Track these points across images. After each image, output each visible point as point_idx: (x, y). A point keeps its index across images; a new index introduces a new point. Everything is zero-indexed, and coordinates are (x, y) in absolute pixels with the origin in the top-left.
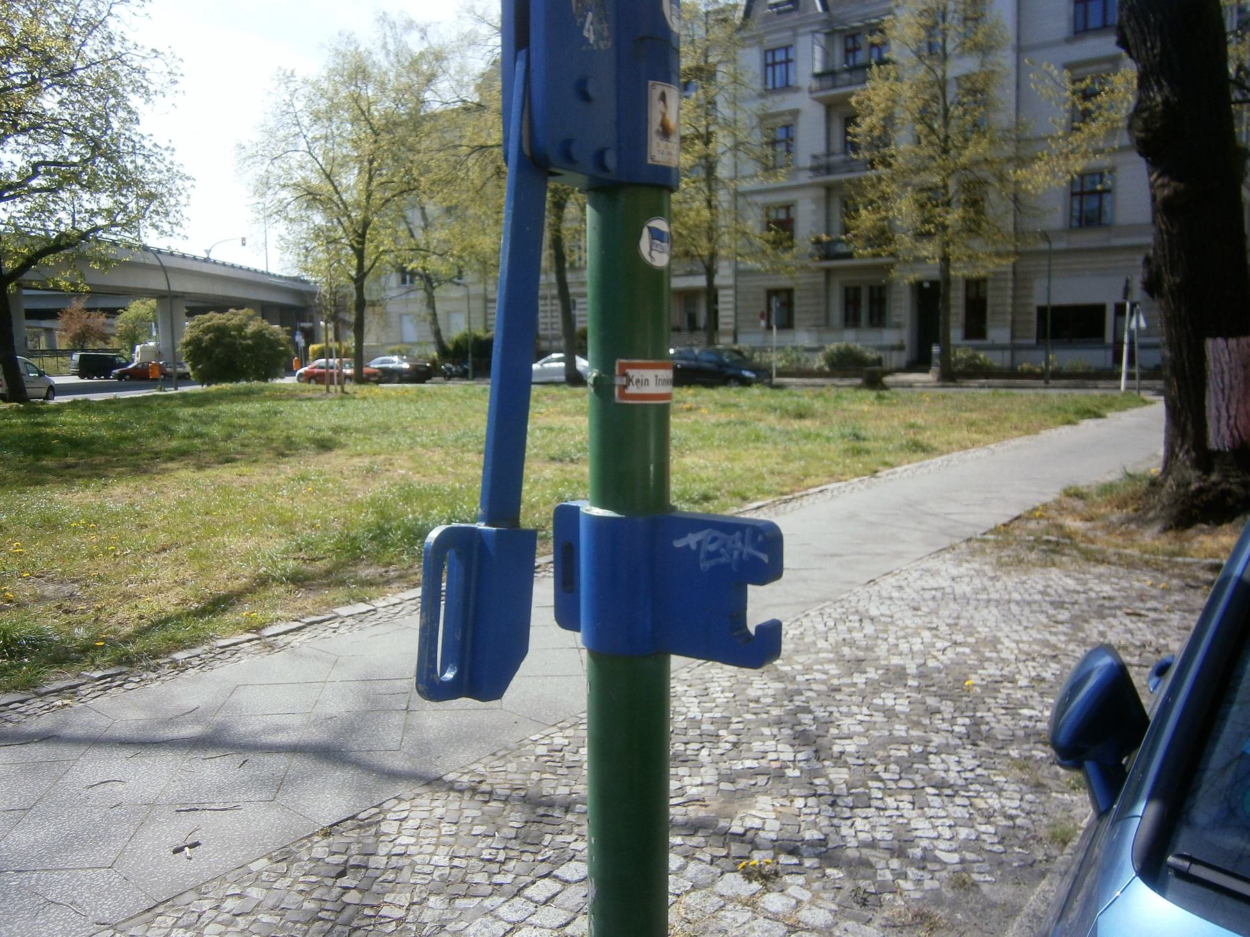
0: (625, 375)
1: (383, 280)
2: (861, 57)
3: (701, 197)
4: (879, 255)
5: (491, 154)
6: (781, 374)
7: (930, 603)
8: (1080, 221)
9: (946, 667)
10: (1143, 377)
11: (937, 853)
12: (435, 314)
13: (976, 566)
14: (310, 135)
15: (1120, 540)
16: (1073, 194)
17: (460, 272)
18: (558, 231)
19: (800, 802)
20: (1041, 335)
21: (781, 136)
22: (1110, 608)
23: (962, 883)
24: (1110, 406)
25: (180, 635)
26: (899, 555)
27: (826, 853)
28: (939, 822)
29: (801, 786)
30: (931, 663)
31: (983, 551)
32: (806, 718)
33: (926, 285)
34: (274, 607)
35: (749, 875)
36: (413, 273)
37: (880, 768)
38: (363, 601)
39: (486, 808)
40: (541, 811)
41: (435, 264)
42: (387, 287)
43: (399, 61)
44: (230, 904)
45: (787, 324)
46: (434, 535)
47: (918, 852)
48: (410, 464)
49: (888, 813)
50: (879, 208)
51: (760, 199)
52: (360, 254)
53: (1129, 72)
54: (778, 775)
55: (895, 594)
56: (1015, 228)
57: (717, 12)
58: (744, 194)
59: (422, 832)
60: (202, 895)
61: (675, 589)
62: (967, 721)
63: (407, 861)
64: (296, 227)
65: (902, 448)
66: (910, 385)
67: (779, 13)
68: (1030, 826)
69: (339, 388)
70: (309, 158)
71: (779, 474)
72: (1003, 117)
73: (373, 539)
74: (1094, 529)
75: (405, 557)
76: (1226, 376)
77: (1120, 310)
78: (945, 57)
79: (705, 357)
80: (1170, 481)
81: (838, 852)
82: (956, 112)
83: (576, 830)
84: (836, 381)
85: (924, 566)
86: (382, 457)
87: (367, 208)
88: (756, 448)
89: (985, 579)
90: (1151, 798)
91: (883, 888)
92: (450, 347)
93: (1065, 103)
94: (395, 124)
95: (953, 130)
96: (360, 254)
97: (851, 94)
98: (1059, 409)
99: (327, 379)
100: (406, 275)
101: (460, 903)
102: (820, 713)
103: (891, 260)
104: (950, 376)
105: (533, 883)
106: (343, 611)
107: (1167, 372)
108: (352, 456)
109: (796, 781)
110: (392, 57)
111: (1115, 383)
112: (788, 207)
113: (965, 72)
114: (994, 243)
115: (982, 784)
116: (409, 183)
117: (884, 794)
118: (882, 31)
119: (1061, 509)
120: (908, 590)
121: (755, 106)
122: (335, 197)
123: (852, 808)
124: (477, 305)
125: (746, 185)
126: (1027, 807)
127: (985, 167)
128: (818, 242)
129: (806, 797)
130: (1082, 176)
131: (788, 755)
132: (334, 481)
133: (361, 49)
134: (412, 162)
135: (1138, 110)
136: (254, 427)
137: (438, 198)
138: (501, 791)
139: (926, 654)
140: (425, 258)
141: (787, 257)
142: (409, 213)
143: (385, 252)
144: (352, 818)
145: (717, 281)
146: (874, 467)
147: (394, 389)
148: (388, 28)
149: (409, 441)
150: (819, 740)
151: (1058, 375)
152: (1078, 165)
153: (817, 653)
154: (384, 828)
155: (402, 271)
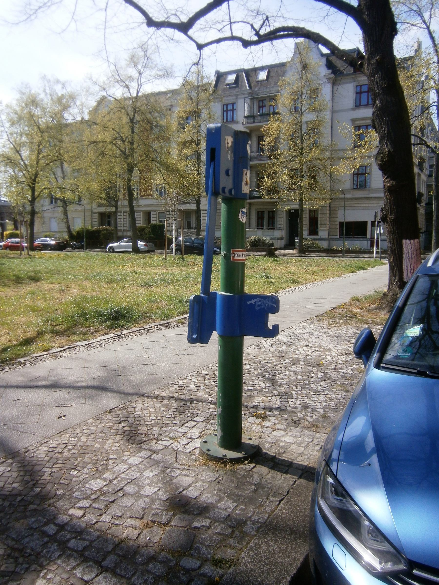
2: (266, 110)
3: (195, 169)
4: (273, 198)
7: (305, 337)
8: (357, 186)
10: (382, 253)
12: (67, 218)
13: (321, 325)
14: (9, 132)
19: (270, 398)
20: (341, 234)
23: (325, 417)
24: (369, 265)
29: (269, 393)
30: (308, 357)
31: (323, 320)
33: (293, 211)
34: (50, 342)
36: (56, 199)
37: (294, 388)
38: (86, 340)
41: (68, 195)
42: (44, 204)
57: (203, 85)
60: (75, 429)
63: (141, 419)
65: (287, 281)
72: (325, 141)
74: (363, 312)
76: (410, 254)
77: (373, 224)
78: (302, 113)
79: (196, 241)
80: (390, 294)
82: (306, 137)
85: (302, 325)
89: (324, 330)
91: (300, 419)
92: (75, 234)
94: (51, 128)
95: (305, 145)
97: (261, 127)
100: (53, 199)
103: (278, 200)
104: (303, 251)
106: (79, 344)
107: (389, 252)
109: (267, 392)
114: (322, 194)
116: (58, 157)
124: (88, 214)
131: (263, 385)
135: (379, 153)
145: (201, 207)
147: (53, 254)
148: (46, 82)
151: (348, 251)
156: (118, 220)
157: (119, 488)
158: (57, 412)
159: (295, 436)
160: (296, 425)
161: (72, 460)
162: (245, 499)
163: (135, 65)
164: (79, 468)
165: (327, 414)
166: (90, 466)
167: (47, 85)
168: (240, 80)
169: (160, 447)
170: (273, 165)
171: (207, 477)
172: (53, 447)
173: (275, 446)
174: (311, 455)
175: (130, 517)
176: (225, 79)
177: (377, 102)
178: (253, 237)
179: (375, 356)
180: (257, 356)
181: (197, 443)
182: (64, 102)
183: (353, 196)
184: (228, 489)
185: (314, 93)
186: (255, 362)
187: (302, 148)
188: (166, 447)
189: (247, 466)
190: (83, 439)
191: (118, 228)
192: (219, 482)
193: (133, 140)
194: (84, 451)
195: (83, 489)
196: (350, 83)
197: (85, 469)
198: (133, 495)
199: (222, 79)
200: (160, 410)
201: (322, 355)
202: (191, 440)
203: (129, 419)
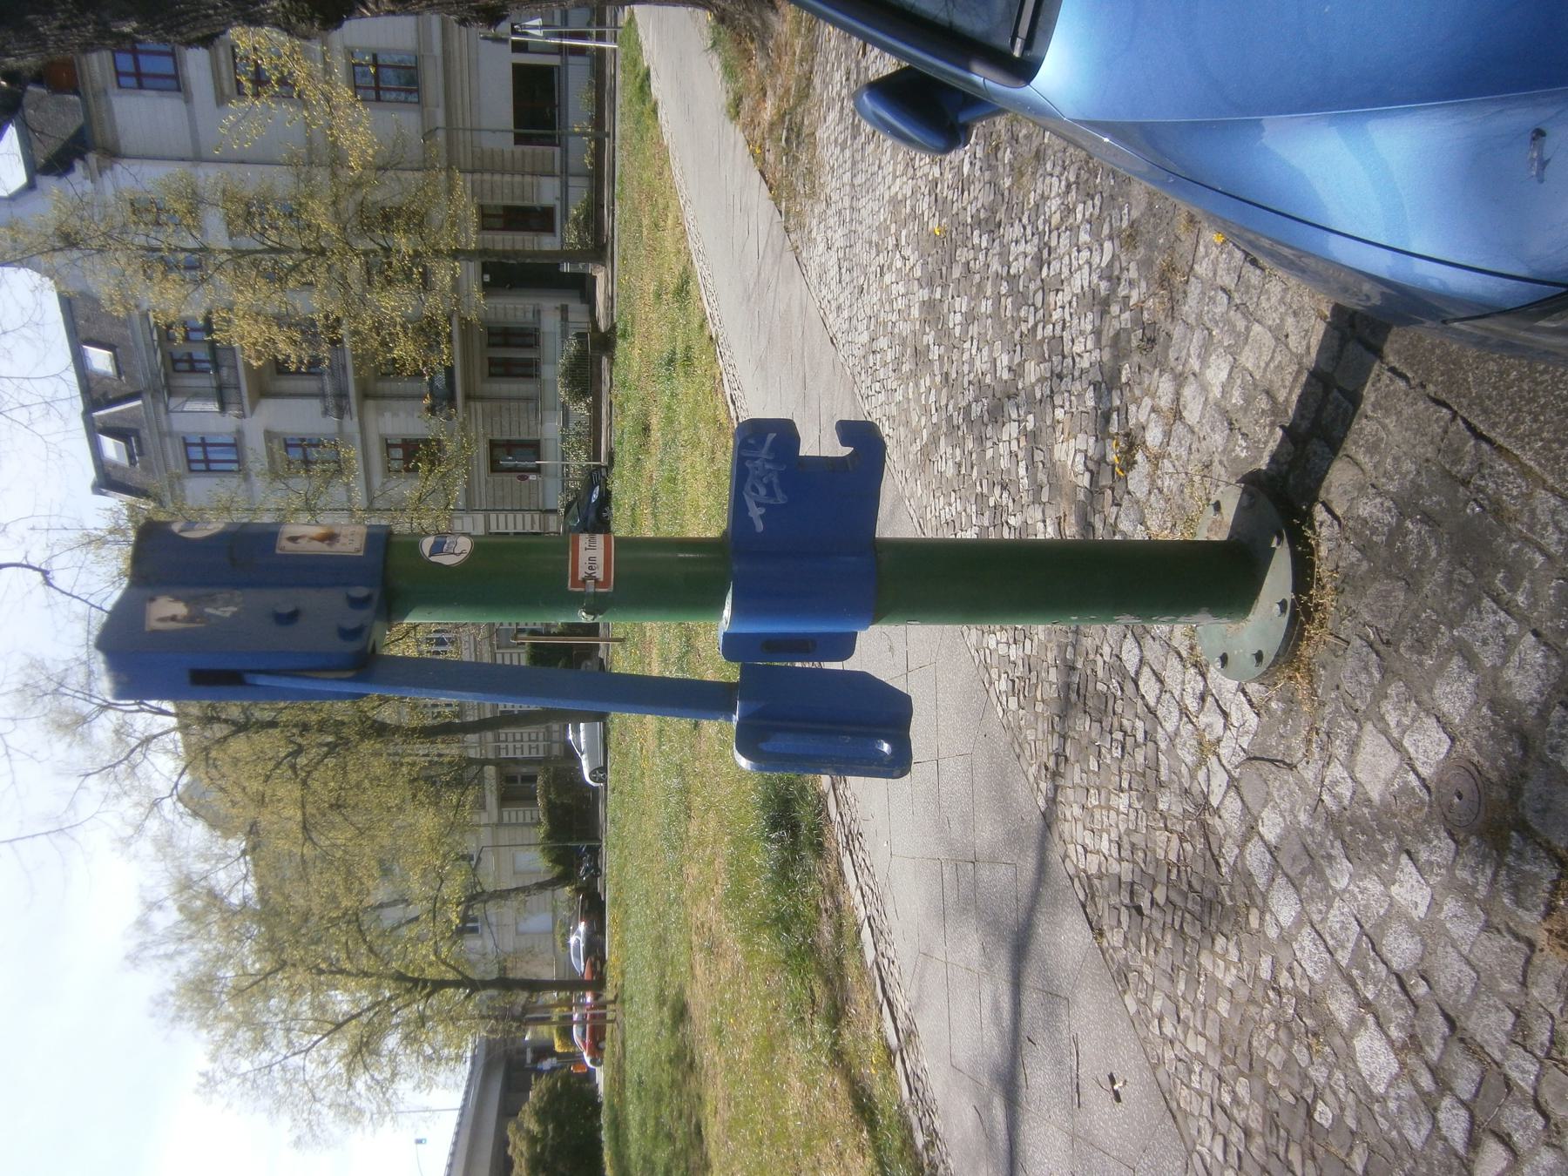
0: (584, 581)
1: (472, 957)
2: (201, 353)
4: (450, 335)
5: (313, 815)
6: (597, 457)
8: (410, 92)
9: (921, 256)
10: (601, 23)
11: (1103, 265)
12: (517, 889)
13: (815, 222)
14: (284, 1051)
15: (786, 59)
16: (378, 99)
17: (463, 857)
18: (414, 730)
20: (550, 141)
21: (298, 454)
22: (858, 73)
23: (1130, 238)
24: (635, 63)
25: (897, 1144)
26: (804, 310)
27: (1107, 382)
28: (1075, 263)
29: (1043, 412)
30: (918, 273)
31: (799, 214)
32: (976, 410)
33: (487, 278)
34: (866, 1038)
35: (1129, 464)
36: (465, 918)
39: (1072, 759)
40: (1073, 697)
41: (453, 889)
42: (481, 952)
43: (191, 937)
44: (1168, 1029)
45: (534, 448)
46: (744, 762)
47: (1104, 285)
48: (703, 904)
49: (1068, 318)
50: (390, 334)
51: (377, 480)
52: (440, 985)
53: (242, 38)
54: (1033, 437)
55: (846, 314)
56: (418, 170)
58: (371, 499)
59: (1097, 826)
60: (1161, 1061)
61: (808, 531)
62: (976, 233)
63: (1125, 839)
64: (403, 1068)
66: (610, 299)
67: (141, 454)
68: (1076, 166)
69: (610, 1007)
70: (313, 1052)
71: (713, 452)
72: (282, 181)
73: (788, 931)
74: (774, 87)
75: (809, 890)
77: (519, 47)
78: (204, 249)
81: (1106, 369)
83: (1091, 657)
84: (605, 389)
85: (815, 282)
86: (694, 938)
87: (380, 976)
88: (684, 481)
89: (829, 212)
90: (968, 70)
91: (1138, 322)
92: (558, 869)
93: (269, 107)
94: (272, 940)
95: (297, 242)
96: (440, 985)
97: (248, 366)
98: (638, 122)
99: (598, 1022)
100: (467, 927)
101: (1164, 774)
102: (970, 395)
104: (599, 250)
105: (1143, 697)
106: (870, 955)
108: (694, 977)
110: (185, 946)
111: (608, 55)
112: (389, 446)
113: (223, 226)
114: (436, 194)
115: (1038, 217)
116: (349, 922)
117: (1049, 322)
118: (169, 327)
119: (753, 123)
120: (841, 300)
121: (259, 484)
122: (364, 1019)
123: (1064, 357)
124: (505, 836)
125: (359, 496)
126: (1058, 170)
127: (342, 206)
128: (432, 410)
129: (1054, 407)
130: (356, 88)
132: (722, 992)
133: (173, 987)
134: (322, 918)
135: (289, 30)
136: (658, 1108)
137: (370, 884)
138: (1055, 744)
139: (908, 279)
140: (445, 902)
141: (450, 447)
142: (387, 924)
143: (436, 953)
144: (1084, 907)
146: (705, 341)
147: (612, 936)
148: (146, 953)
149: (675, 907)
150: (998, 395)
151: (598, 121)
152: (344, 93)
153: (909, 400)
154: (1093, 870)
155: (461, 932)
156: (518, 755)
157: (1396, 987)
158: (1096, 1097)
159: (1207, 347)
160: (1162, 338)
161: (1276, 1106)
162: (1463, 564)
163: (83, 720)
164: (1308, 1093)
165: (1121, 232)
166: (1302, 1056)
167: (153, 952)
168: (119, 423)
169: (1233, 806)
170: (355, 333)
171: (1363, 678)
172: (1225, 1153)
173: (1244, 422)
174: (1282, 301)
175: (1524, 984)
176: (115, 466)
177: (127, 30)
178: (562, 391)
179: (982, 77)
180: (916, 434)
181: (1225, 686)
182: (201, 905)
183: (442, 104)
184: (1417, 617)
185: (146, 210)
186: (934, 441)
187: (305, 250)
188: (1233, 784)
189: (1325, 532)
190: (1197, 1045)
191: (541, 755)
192: (1388, 643)
193: (295, 726)
194: (1236, 1053)
195: (1392, 1105)
196: (110, 109)
197: (1312, 1072)
198: (1425, 945)
199: (116, 476)
200: (1097, 774)
201: (914, 227)
202: (1209, 699)
203: (1127, 878)
